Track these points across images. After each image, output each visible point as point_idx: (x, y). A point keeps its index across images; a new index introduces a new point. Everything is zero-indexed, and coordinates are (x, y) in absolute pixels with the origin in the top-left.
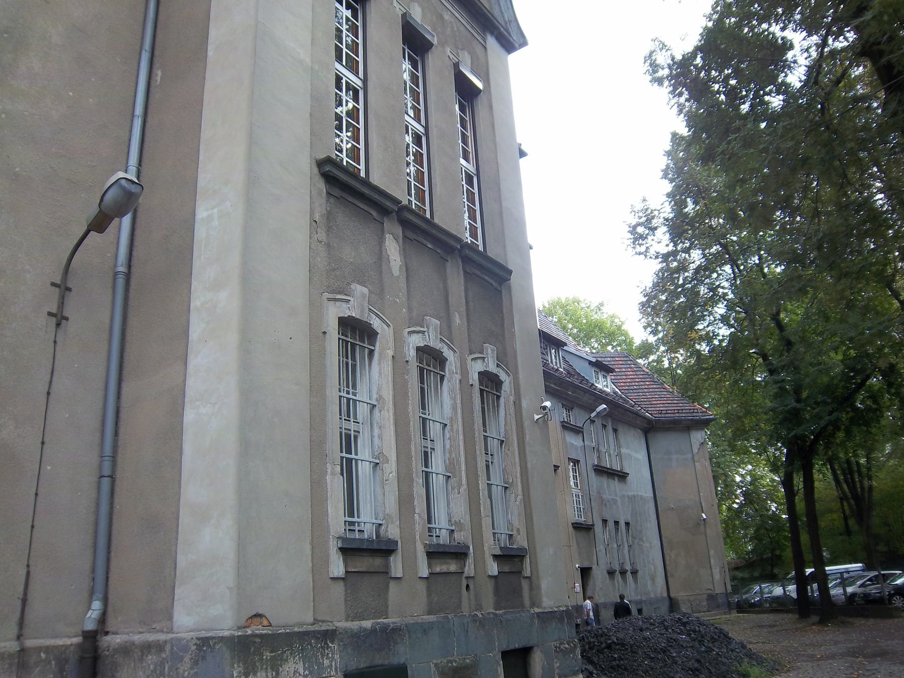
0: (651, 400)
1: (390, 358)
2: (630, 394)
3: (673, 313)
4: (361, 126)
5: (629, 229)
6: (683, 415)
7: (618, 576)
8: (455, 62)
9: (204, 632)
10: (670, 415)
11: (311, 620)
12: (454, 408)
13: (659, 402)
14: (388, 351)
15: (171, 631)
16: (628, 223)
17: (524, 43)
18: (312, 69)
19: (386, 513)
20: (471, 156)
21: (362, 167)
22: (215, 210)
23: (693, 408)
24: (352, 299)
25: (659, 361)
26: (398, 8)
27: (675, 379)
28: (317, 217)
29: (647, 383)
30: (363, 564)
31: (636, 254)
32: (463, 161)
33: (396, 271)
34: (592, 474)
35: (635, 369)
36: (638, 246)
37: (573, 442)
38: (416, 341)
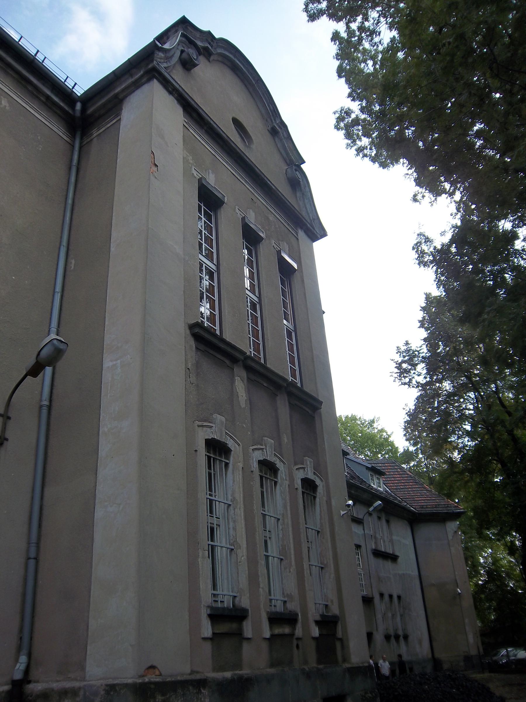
0: (414, 497)
1: (241, 469)
2: (398, 493)
3: (432, 429)
4: (216, 298)
5: (396, 365)
6: (440, 509)
7: (393, 640)
8: (278, 250)
9: (111, 680)
10: (429, 509)
11: (189, 671)
12: (285, 507)
13: (420, 499)
14: (239, 464)
15: (84, 679)
16: (396, 360)
17: (324, 234)
18: (184, 259)
19: (240, 587)
20: (290, 317)
21: (217, 328)
22: (119, 361)
23: (447, 503)
24: (214, 425)
25: (418, 465)
26: (239, 214)
27: (431, 481)
28: (189, 366)
29: (411, 484)
30: (224, 628)
31: (402, 384)
32: (285, 322)
33: (243, 404)
34: (371, 557)
35: (401, 473)
36: (403, 378)
37: (356, 531)
38: (258, 456)
